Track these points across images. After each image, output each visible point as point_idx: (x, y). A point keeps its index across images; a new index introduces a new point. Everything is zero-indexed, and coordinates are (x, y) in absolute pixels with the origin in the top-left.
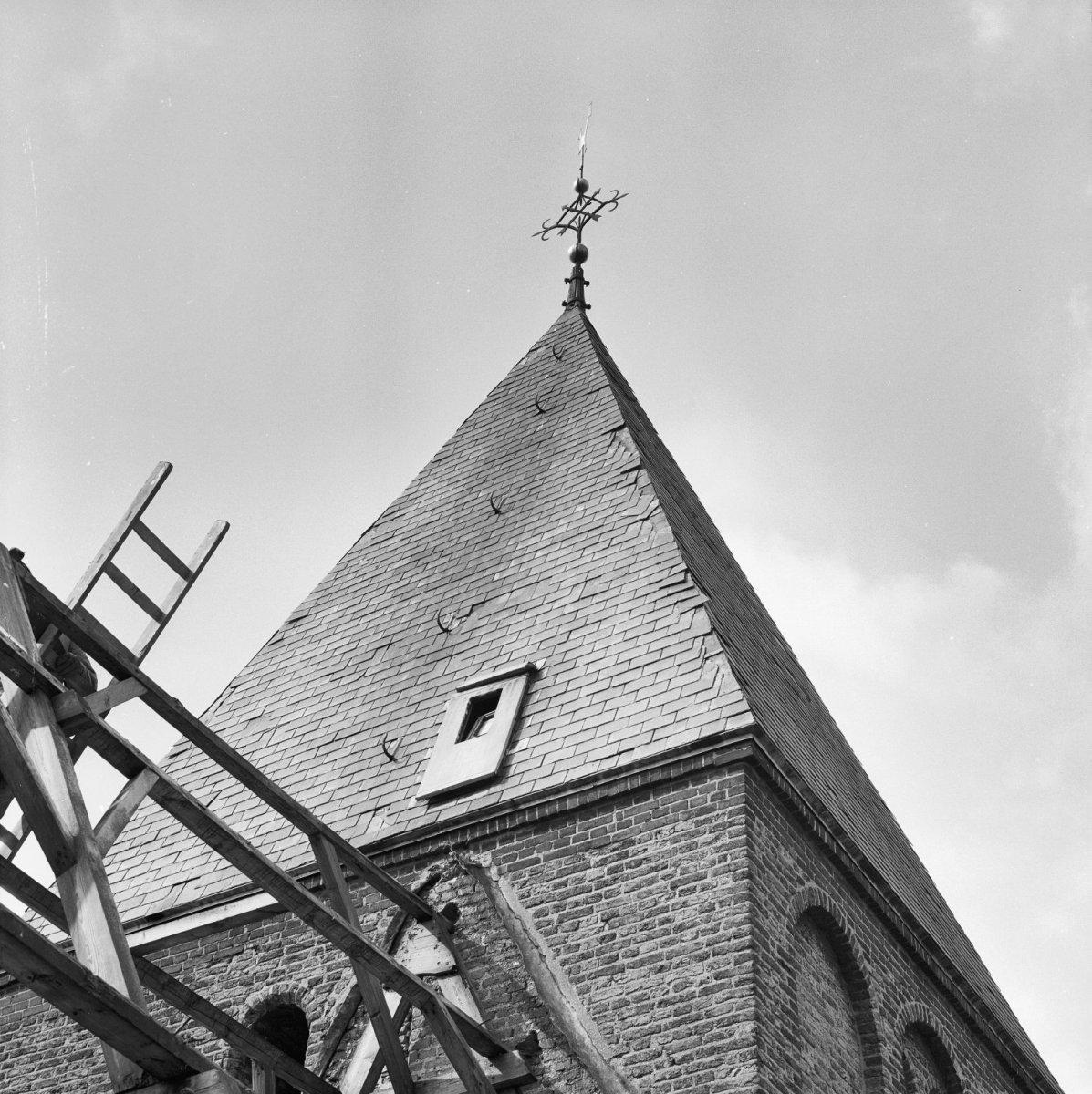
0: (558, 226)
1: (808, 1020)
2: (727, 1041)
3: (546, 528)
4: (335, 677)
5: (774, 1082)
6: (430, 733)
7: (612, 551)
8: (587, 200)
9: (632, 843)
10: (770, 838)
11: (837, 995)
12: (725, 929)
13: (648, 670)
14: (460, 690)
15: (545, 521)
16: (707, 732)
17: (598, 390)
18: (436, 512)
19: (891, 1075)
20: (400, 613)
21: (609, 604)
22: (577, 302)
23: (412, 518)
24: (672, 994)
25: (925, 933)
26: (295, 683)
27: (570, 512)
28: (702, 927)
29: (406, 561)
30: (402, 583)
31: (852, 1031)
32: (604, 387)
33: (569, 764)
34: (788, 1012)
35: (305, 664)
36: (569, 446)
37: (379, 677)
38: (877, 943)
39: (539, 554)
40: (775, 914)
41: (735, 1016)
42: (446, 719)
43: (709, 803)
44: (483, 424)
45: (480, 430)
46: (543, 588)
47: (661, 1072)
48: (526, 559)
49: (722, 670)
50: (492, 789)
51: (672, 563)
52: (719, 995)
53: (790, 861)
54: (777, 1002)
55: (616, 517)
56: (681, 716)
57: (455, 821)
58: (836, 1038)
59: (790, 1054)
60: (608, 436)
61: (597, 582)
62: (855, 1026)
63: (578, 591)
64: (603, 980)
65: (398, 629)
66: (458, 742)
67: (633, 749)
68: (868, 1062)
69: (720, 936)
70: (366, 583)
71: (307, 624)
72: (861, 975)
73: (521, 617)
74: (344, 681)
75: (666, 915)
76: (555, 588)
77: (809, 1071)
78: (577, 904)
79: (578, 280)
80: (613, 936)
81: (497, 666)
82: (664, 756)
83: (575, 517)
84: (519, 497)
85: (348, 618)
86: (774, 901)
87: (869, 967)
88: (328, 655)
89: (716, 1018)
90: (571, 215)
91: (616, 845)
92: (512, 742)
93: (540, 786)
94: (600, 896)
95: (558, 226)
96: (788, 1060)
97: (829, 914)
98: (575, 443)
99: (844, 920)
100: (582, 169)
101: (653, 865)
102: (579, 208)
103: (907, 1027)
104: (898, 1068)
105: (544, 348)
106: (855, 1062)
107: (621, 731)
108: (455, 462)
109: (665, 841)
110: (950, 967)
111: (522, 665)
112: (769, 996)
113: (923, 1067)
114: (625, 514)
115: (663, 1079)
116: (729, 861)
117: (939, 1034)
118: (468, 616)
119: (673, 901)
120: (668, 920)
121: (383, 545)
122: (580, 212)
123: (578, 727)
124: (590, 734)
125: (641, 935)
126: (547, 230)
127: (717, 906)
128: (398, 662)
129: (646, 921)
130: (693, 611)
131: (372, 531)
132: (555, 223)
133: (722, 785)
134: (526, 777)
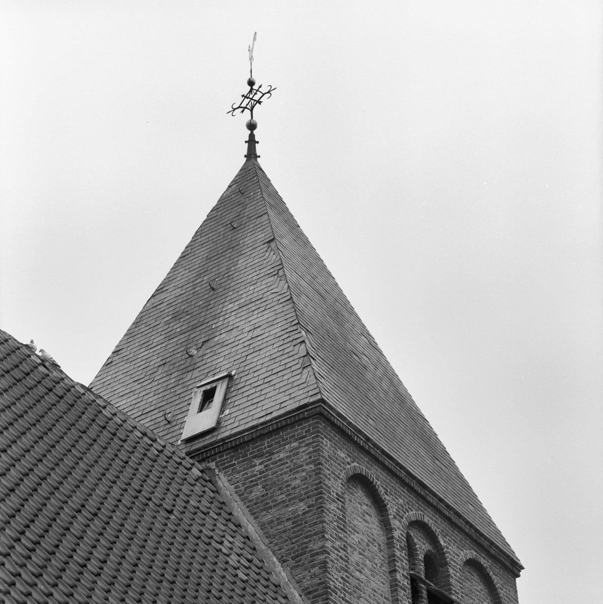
0: (239, 107)
1: (355, 522)
2: (313, 532)
3: (236, 299)
4: (140, 381)
5: (333, 547)
6: (185, 409)
7: (267, 312)
8: (255, 91)
9: (274, 454)
10: (332, 446)
11: (372, 511)
12: (311, 487)
13: (280, 374)
14: (198, 387)
15: (236, 295)
16: (302, 403)
17: (262, 216)
18: (184, 288)
19: (398, 544)
20: (169, 347)
21: (264, 341)
22: (252, 155)
23: (169, 296)
24: (291, 516)
25: (419, 480)
26: (121, 385)
27: (247, 290)
28: (303, 487)
29: (170, 317)
30: (169, 330)
31: (380, 526)
32: (264, 214)
33: (246, 420)
34: (341, 519)
35: (124, 375)
36: (247, 250)
37: (161, 381)
38: (392, 487)
39: (233, 314)
40: (334, 479)
41: (316, 522)
42: (193, 401)
43: (304, 434)
44: (206, 234)
45: (204, 238)
46: (235, 333)
47: (288, 547)
48: (227, 316)
49: (310, 373)
50: (214, 434)
51: (292, 319)
52: (310, 514)
53: (343, 455)
54: (335, 515)
55: (268, 293)
56: (292, 396)
57: (198, 450)
58: (371, 529)
59: (342, 536)
60: (265, 245)
61: (259, 329)
62: (382, 524)
63: (251, 334)
64: (264, 513)
65: (168, 355)
66: (198, 413)
67: (272, 412)
68: (388, 539)
69: (310, 490)
70: (151, 330)
71: (124, 353)
72: (383, 501)
73: (225, 348)
74: (144, 384)
75: (288, 483)
76: (240, 332)
77: (355, 543)
78: (252, 481)
79: (252, 142)
80: (267, 494)
81: (214, 374)
82: (285, 415)
83: (249, 293)
84: (223, 280)
85: (143, 350)
86: (334, 474)
87: (388, 498)
88: (136, 370)
89: (309, 524)
90: (247, 101)
91: (267, 455)
92: (222, 411)
93: (234, 431)
94: (261, 477)
95: (239, 107)
96: (340, 538)
97: (365, 476)
98: (250, 249)
99: (373, 478)
100: (251, 72)
101: (282, 462)
102: (251, 97)
103: (409, 523)
104: (403, 540)
105: (236, 185)
106: (382, 539)
107: (268, 404)
108: (192, 258)
109: (287, 452)
110: (435, 495)
111: (225, 374)
112: (331, 513)
113: (422, 540)
114: (272, 291)
115: (289, 550)
116: (313, 458)
117: (430, 525)
118: (201, 348)
119: (291, 477)
120: (289, 486)
121: (158, 307)
122: (251, 99)
123: (250, 403)
124: (255, 406)
125: (279, 492)
126: (234, 109)
127: (308, 478)
128: (169, 373)
129: (280, 486)
130: (299, 345)
131: (152, 299)
132: (238, 106)
133: (309, 426)
134: (229, 427)
